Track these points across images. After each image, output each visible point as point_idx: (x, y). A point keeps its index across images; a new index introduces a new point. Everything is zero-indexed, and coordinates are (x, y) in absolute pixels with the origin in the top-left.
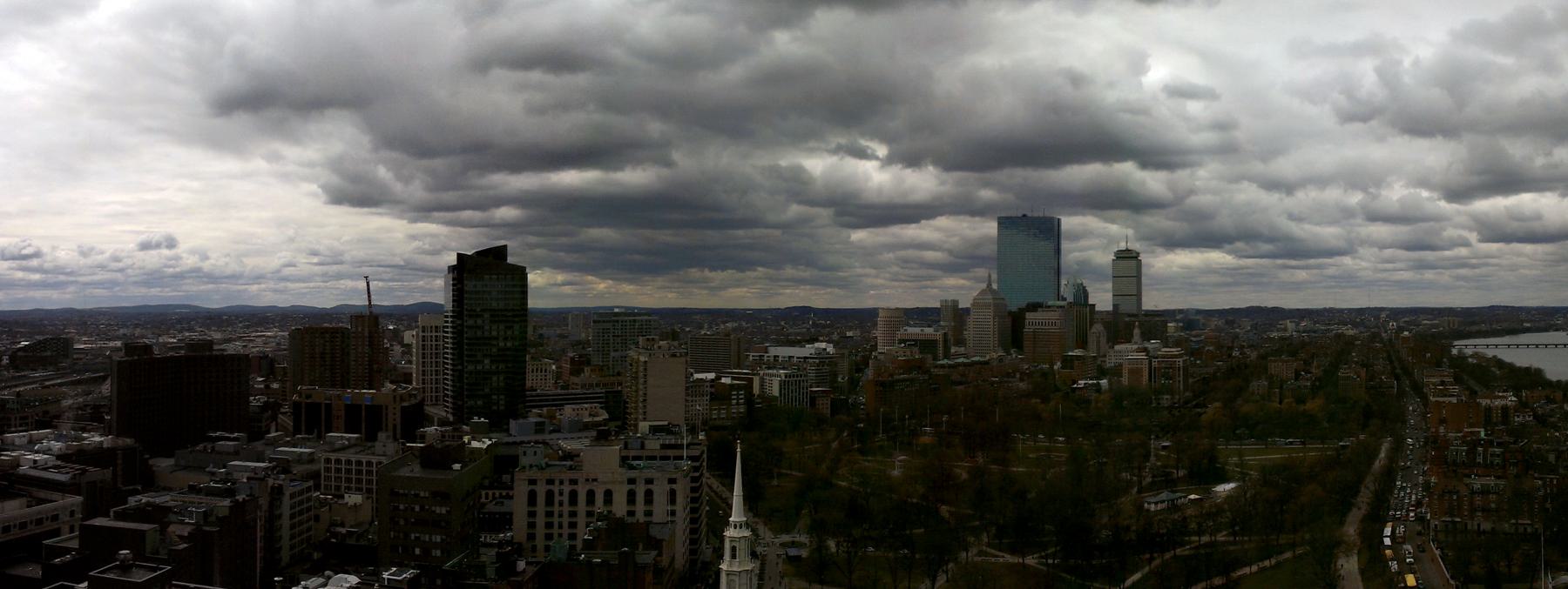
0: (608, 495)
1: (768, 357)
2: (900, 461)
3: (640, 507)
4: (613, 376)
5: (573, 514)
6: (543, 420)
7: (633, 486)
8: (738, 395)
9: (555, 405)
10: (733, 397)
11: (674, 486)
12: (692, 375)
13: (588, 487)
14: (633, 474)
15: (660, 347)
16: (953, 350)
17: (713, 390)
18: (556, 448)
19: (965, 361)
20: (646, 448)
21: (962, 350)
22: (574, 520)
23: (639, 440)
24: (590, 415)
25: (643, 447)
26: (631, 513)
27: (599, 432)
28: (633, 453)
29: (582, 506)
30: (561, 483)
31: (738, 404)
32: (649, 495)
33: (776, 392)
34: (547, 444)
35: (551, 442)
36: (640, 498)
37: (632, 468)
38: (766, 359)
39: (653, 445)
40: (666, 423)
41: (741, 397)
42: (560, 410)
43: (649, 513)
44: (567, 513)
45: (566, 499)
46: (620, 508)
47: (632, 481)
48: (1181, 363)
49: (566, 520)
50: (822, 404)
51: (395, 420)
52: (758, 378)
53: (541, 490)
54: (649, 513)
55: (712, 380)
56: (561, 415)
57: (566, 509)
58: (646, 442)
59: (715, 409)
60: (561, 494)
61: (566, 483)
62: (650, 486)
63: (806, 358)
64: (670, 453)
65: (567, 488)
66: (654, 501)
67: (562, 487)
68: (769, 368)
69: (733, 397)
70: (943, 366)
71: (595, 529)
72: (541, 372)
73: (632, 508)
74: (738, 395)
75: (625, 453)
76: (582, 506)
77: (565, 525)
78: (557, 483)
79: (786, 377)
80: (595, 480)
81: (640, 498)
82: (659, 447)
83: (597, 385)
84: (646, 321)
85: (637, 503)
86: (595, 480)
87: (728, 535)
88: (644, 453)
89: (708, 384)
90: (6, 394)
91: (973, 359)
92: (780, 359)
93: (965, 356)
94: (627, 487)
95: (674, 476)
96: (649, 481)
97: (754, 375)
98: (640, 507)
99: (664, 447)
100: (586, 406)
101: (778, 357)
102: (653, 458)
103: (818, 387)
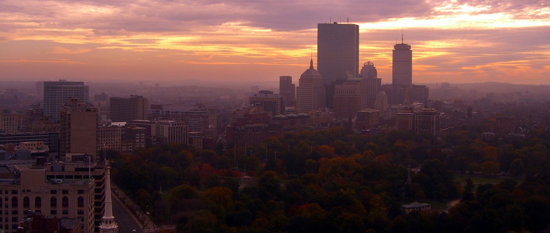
0: (38, 201)
1: (163, 112)
2: (245, 179)
3: (60, 208)
4: (55, 123)
5: (15, 212)
6: (5, 151)
7: (54, 195)
8: (140, 136)
9: (13, 142)
10: (137, 138)
11: (82, 195)
12: (110, 123)
13: (25, 195)
14: (53, 187)
15: (79, 105)
16: (286, 108)
17: (124, 133)
18: (12, 170)
19: (295, 115)
20: (65, 170)
21: (293, 108)
22: (15, 216)
23: (61, 165)
24: (37, 149)
25: (63, 169)
26: (54, 212)
27: (38, 160)
28: (56, 174)
29: (21, 208)
30: (7, 192)
31: (140, 142)
32: (65, 200)
33: (166, 134)
34: (6, 167)
35: (9, 166)
36: (59, 202)
37: (54, 183)
38: (161, 113)
39: (70, 169)
40: (83, 154)
41: (139, 137)
42: (18, 145)
43: (65, 212)
44: (11, 212)
45: (10, 202)
46: (46, 210)
47: (53, 192)
48: (435, 118)
49: (10, 216)
50: (197, 142)
51: (397, 123)
52: (154, 125)
53: (60, 197)
54: (65, 212)
55: (123, 127)
56: (18, 148)
57: (10, 209)
58: (66, 167)
59: (125, 146)
60: (7, 200)
61: (10, 193)
62: (66, 195)
63: (187, 113)
64: (81, 173)
65: (10, 196)
66: (42, 204)
67: (7, 195)
68: (163, 119)
69: (137, 138)
70: (279, 119)
71: (25, 222)
72: (10, 118)
73: (54, 209)
74: (140, 136)
75: (50, 174)
76: (21, 208)
77: (10, 219)
78: (4, 192)
79: (173, 125)
80: (28, 191)
81: (59, 202)
82: (74, 170)
83: (44, 129)
84: (64, 88)
85: (19, 204)
86: (28, 191)
87: (102, 228)
88: (64, 174)
89: (121, 129)
90: (1, 94)
91: (299, 114)
92: (170, 113)
93: (295, 112)
94: (50, 196)
95: (82, 189)
96: (65, 192)
97: (151, 123)
98: (60, 208)
99: (77, 170)
100: (35, 142)
101: (169, 112)
102: (71, 177)
103: (196, 131)
